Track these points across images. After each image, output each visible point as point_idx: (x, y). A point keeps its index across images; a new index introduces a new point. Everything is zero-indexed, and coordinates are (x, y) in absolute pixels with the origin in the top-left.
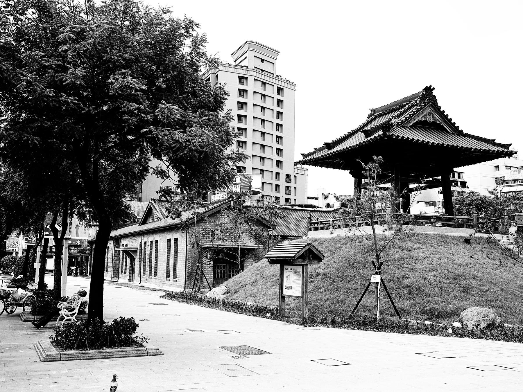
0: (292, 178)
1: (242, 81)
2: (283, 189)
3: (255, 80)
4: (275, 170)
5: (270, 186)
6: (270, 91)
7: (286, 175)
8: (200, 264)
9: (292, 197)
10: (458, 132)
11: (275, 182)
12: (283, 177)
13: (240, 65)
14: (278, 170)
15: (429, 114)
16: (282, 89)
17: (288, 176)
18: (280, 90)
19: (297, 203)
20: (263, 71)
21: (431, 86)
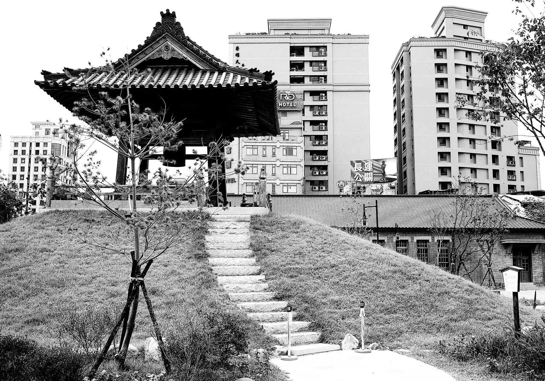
2: (503, 174)
3: (456, 50)
4: (491, 152)
5: (485, 172)
7: (508, 157)
9: (518, 184)
10: (214, 66)
11: (492, 167)
12: (503, 160)
13: (440, 36)
14: (495, 152)
17: (510, 159)
21: (271, 71)
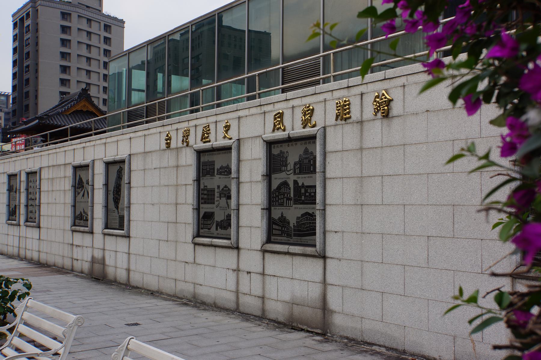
1: (66, 17)
3: (79, 16)
6: (95, 28)
8: (162, 297)
15: (85, 106)
16: (110, 26)
18: (107, 28)
20: (87, 7)
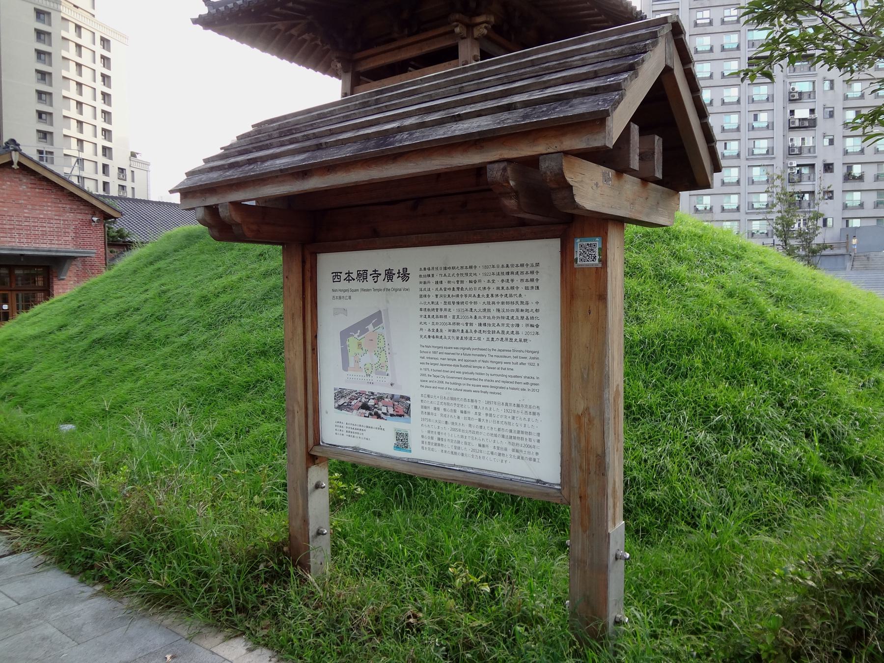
0: (128, 173)
4: (101, 160)
9: (128, 184)
14: (106, 161)
17: (122, 170)
19: (137, 197)
